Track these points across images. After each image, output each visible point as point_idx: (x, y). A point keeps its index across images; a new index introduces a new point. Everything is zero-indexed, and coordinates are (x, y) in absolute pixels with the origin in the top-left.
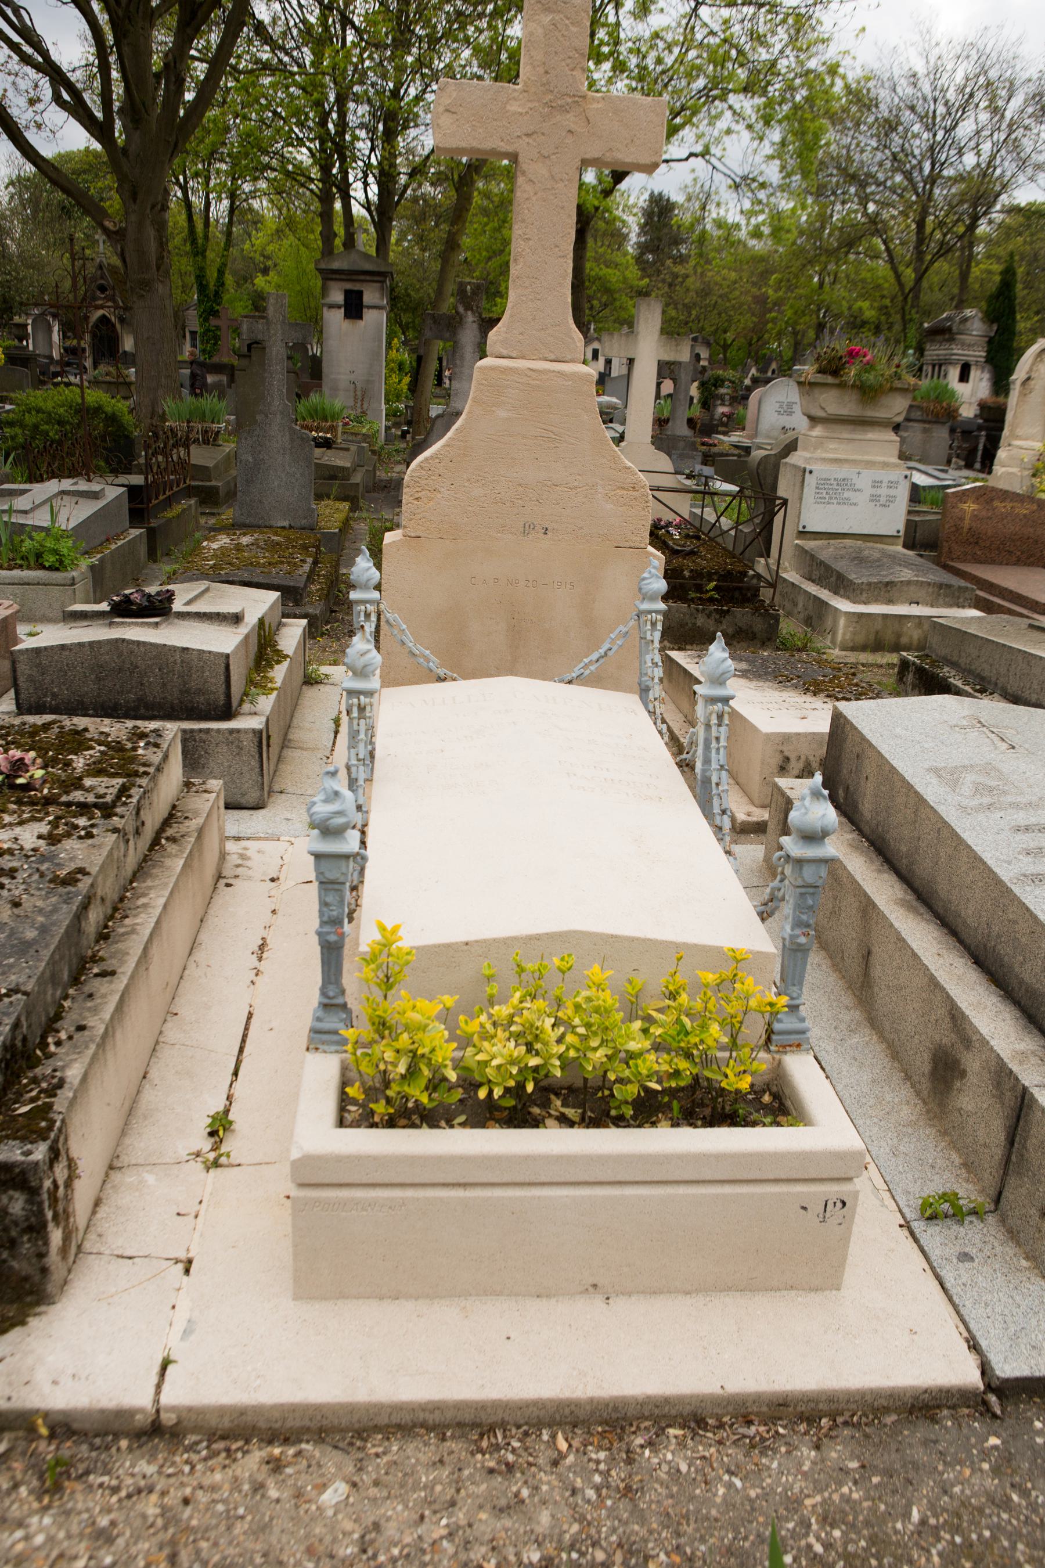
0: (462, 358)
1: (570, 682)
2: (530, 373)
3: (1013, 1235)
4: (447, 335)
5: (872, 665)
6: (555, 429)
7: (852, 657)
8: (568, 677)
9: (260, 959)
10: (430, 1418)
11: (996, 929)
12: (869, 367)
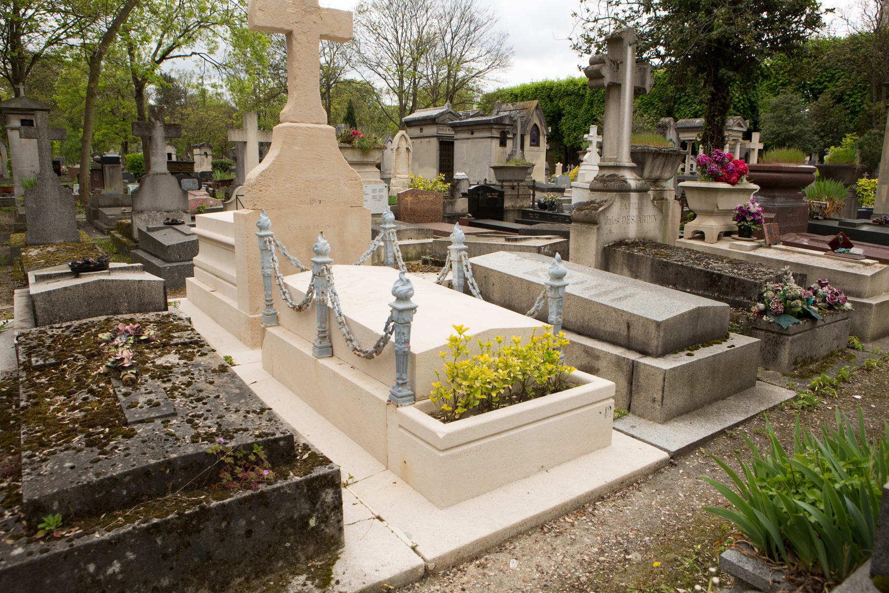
0: (156, 145)
3: (641, 416)
10: (522, 529)
11: (586, 318)
12: (363, 139)
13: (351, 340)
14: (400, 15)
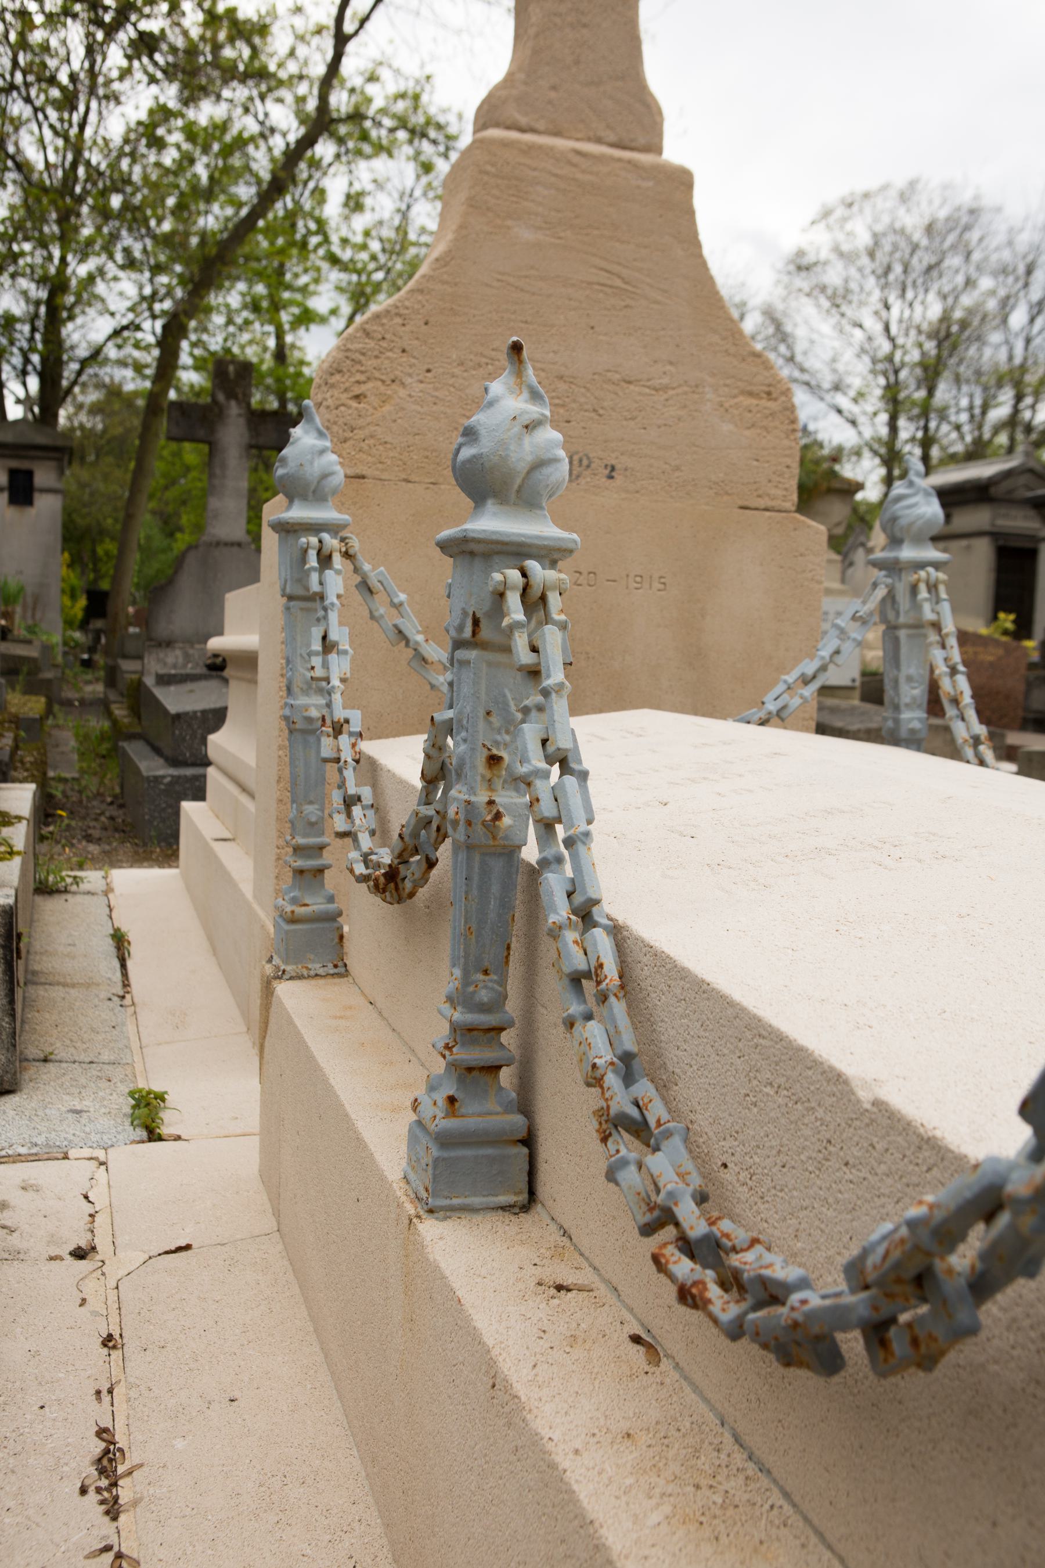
1: (763, 723)
2: (576, 159)
4: (201, 433)
6: (625, 272)
9: (113, 1510)
13: (639, 1129)
14: (898, 269)
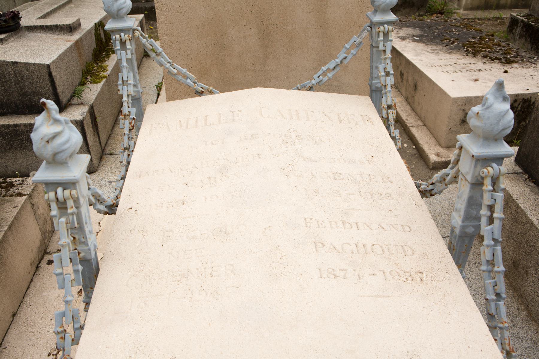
1: (311, 89)
5: (484, 19)
7: (472, 14)
8: (309, 83)
